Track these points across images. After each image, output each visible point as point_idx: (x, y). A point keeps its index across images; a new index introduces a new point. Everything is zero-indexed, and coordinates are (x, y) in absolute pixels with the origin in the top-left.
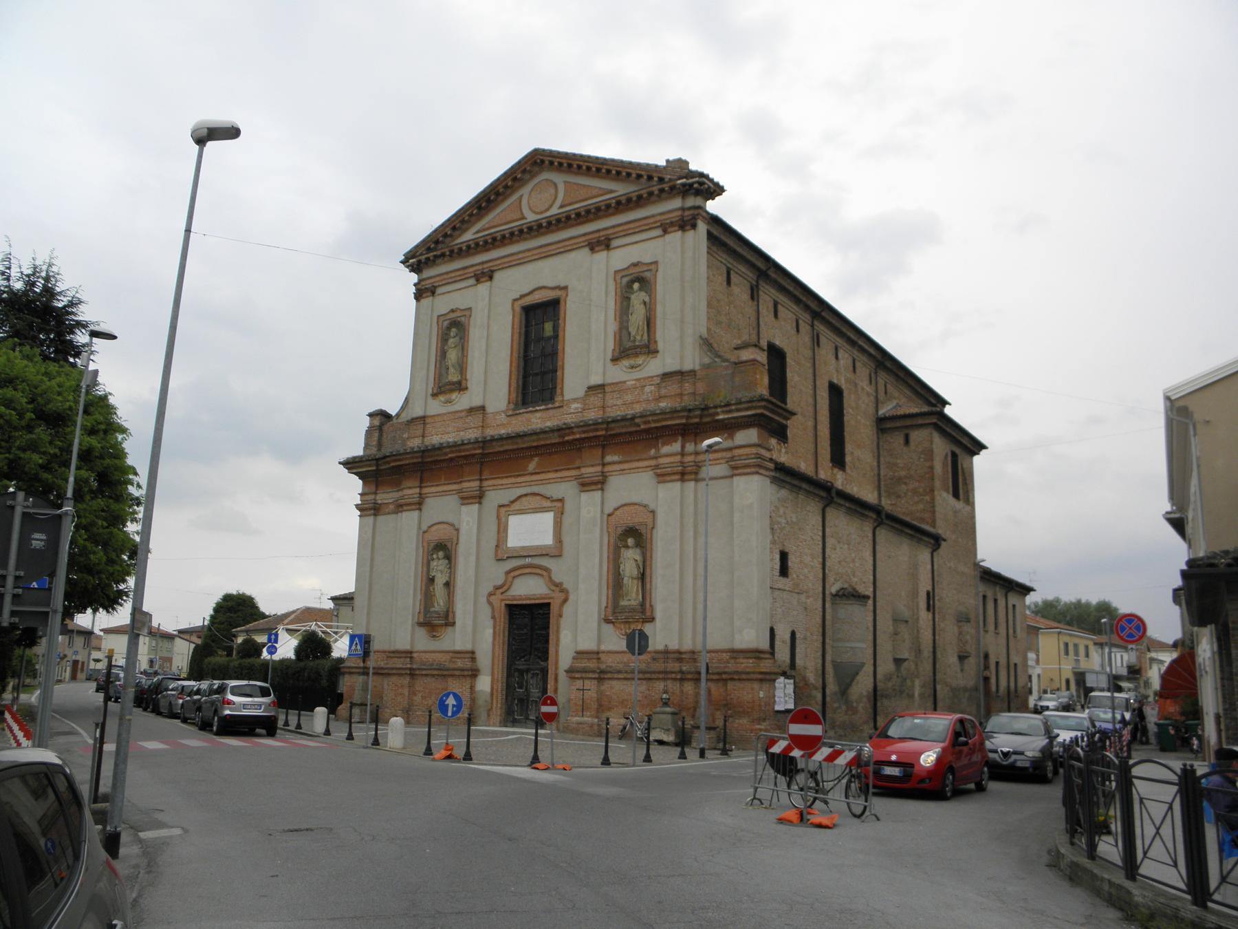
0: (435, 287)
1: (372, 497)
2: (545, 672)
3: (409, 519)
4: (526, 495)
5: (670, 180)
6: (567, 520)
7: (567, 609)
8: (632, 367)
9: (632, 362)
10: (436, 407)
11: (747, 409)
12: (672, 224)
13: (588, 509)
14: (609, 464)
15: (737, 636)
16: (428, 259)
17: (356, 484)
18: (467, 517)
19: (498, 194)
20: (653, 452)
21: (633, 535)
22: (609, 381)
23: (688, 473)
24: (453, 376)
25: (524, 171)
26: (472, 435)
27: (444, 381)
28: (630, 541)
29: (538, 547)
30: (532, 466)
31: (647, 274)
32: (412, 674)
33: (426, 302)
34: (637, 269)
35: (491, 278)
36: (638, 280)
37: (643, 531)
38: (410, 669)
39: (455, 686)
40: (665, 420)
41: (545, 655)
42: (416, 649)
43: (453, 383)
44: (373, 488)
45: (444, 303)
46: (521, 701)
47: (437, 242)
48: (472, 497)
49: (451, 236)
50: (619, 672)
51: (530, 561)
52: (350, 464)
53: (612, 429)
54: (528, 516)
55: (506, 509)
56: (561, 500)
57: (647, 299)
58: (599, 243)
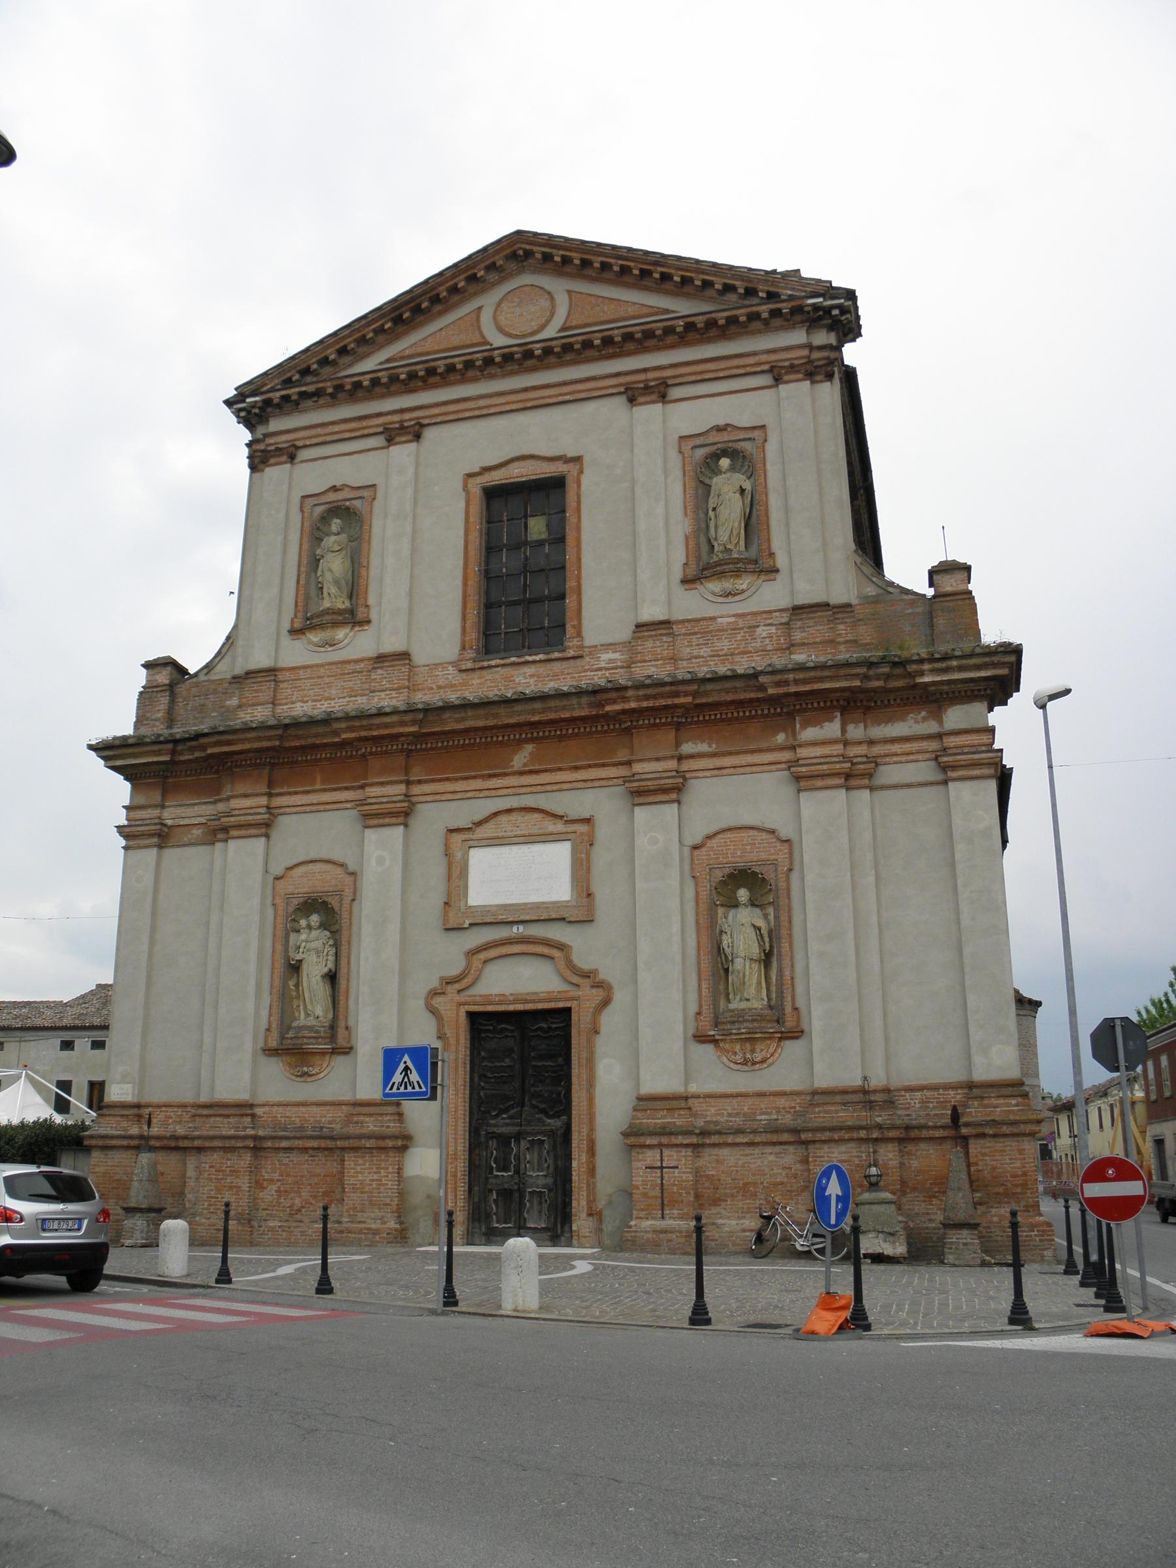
0: (298, 448)
1: (155, 812)
2: (565, 1136)
3: (244, 857)
4: (509, 811)
5: (791, 298)
6: (602, 858)
7: (610, 1020)
8: (728, 594)
9: (728, 584)
10: (297, 653)
11: (978, 667)
12: (793, 368)
13: (657, 831)
14: (692, 756)
15: (977, 1059)
16: (286, 398)
17: (120, 789)
18: (381, 854)
19: (417, 310)
20: (781, 738)
21: (745, 882)
22: (677, 615)
23: (855, 775)
24: (334, 599)
25: (492, 267)
26: (388, 701)
27: (314, 609)
28: (743, 894)
29: (537, 906)
30: (520, 759)
31: (747, 446)
32: (257, 1147)
33: (275, 473)
34: (725, 437)
35: (418, 437)
36: (725, 453)
37: (770, 875)
38: (255, 1138)
39: (360, 1172)
40: (821, 679)
41: (561, 1104)
42: (261, 1099)
43: (340, 612)
44: (157, 797)
45: (316, 474)
46: (506, 1194)
47: (306, 372)
48: (391, 814)
49: (334, 363)
50: (739, 1131)
51: (521, 931)
52: (110, 751)
53: (706, 693)
54: (515, 848)
55: (464, 836)
56: (588, 821)
57: (747, 485)
58: (647, 389)
